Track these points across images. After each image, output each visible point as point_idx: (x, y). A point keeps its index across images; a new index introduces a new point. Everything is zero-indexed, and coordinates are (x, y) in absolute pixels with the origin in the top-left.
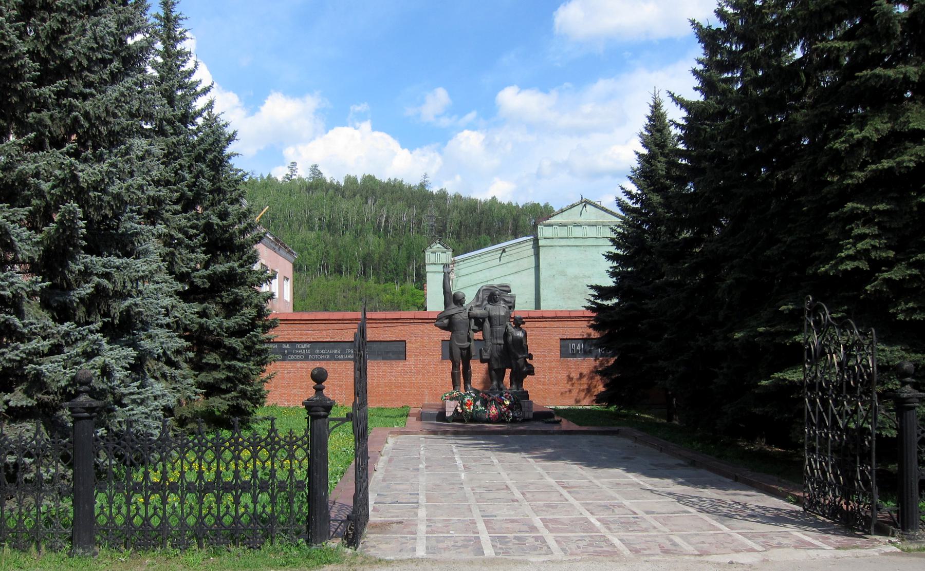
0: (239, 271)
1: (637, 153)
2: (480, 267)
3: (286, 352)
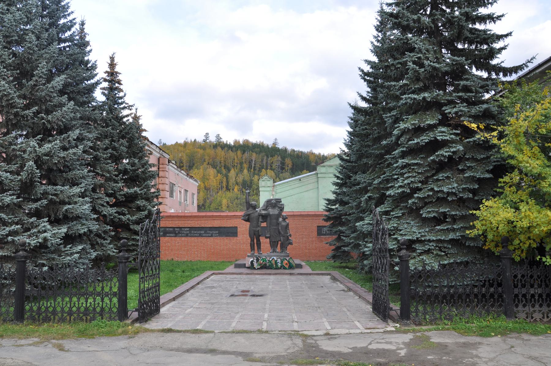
0: (139, 192)
1: (347, 131)
3: (177, 232)
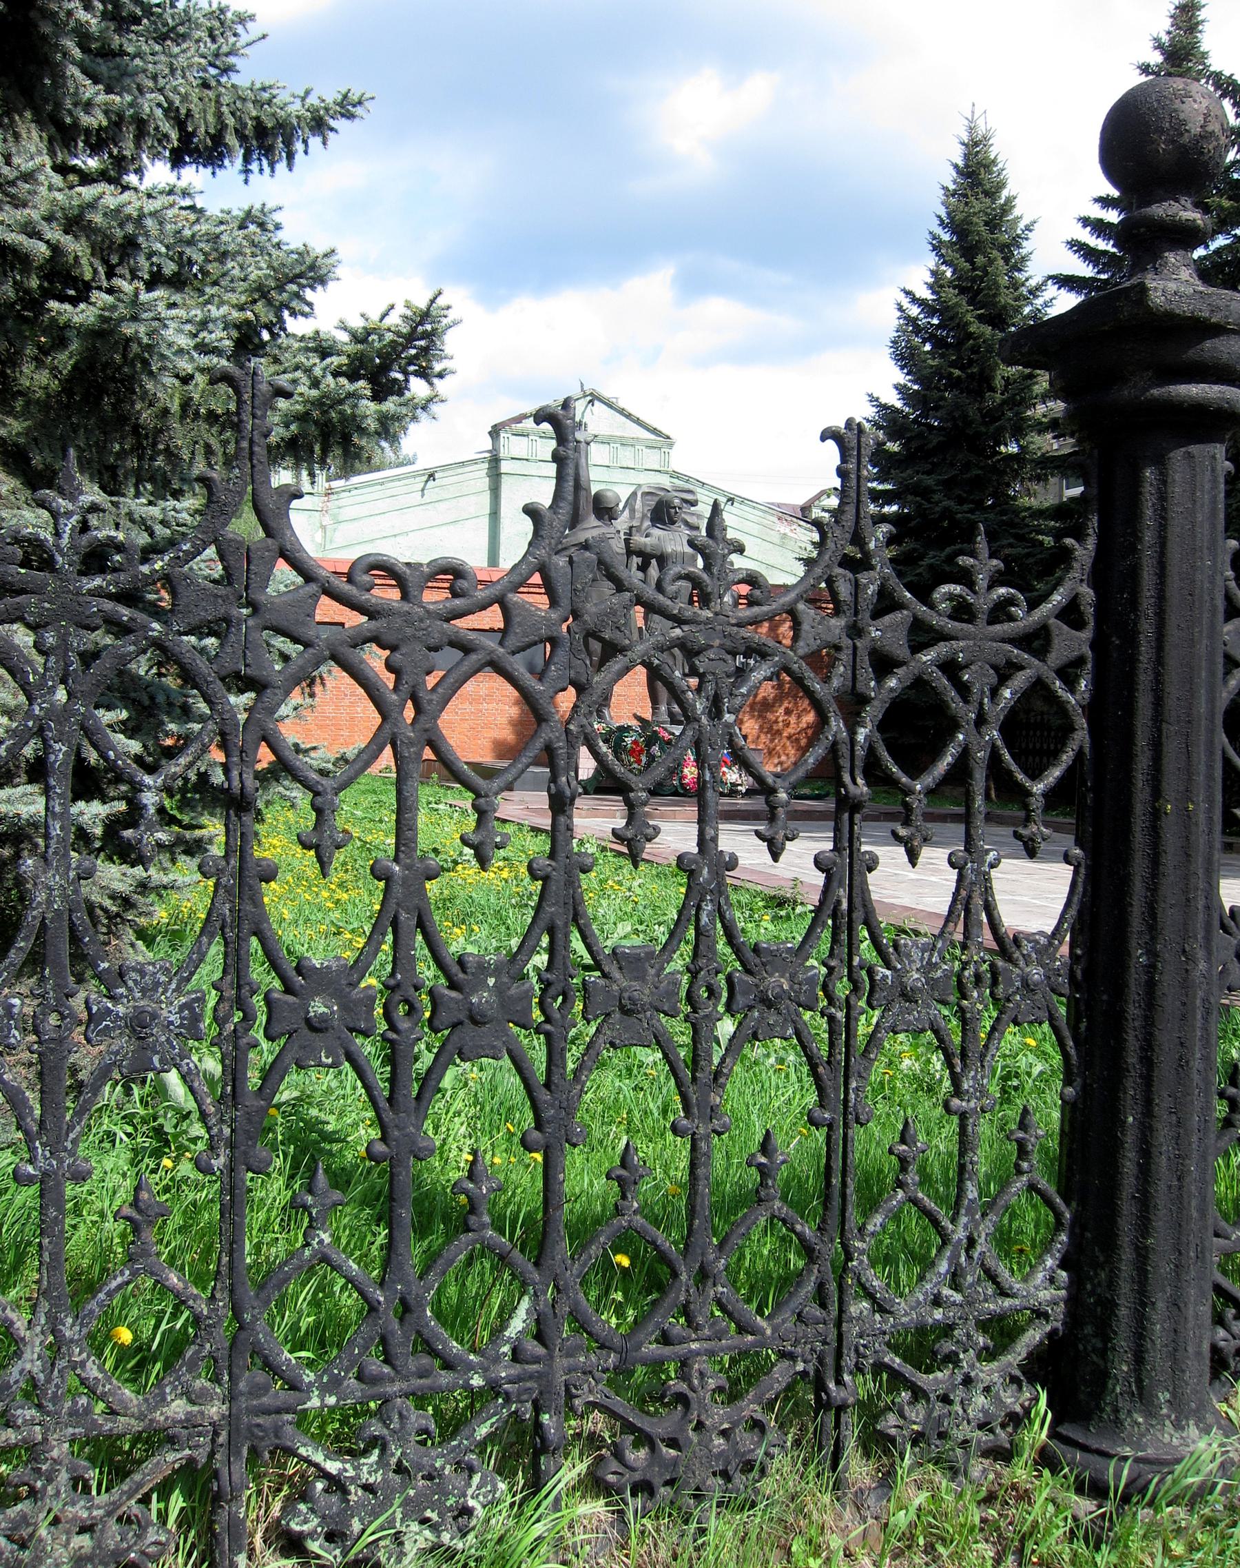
2: (382, 506)
